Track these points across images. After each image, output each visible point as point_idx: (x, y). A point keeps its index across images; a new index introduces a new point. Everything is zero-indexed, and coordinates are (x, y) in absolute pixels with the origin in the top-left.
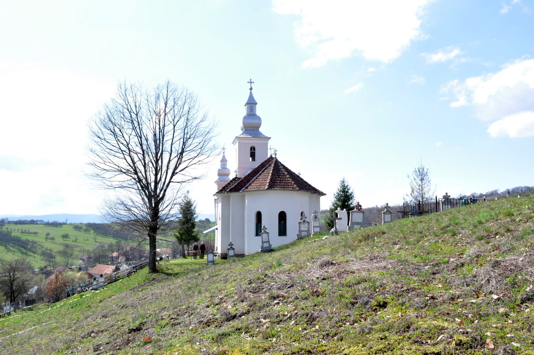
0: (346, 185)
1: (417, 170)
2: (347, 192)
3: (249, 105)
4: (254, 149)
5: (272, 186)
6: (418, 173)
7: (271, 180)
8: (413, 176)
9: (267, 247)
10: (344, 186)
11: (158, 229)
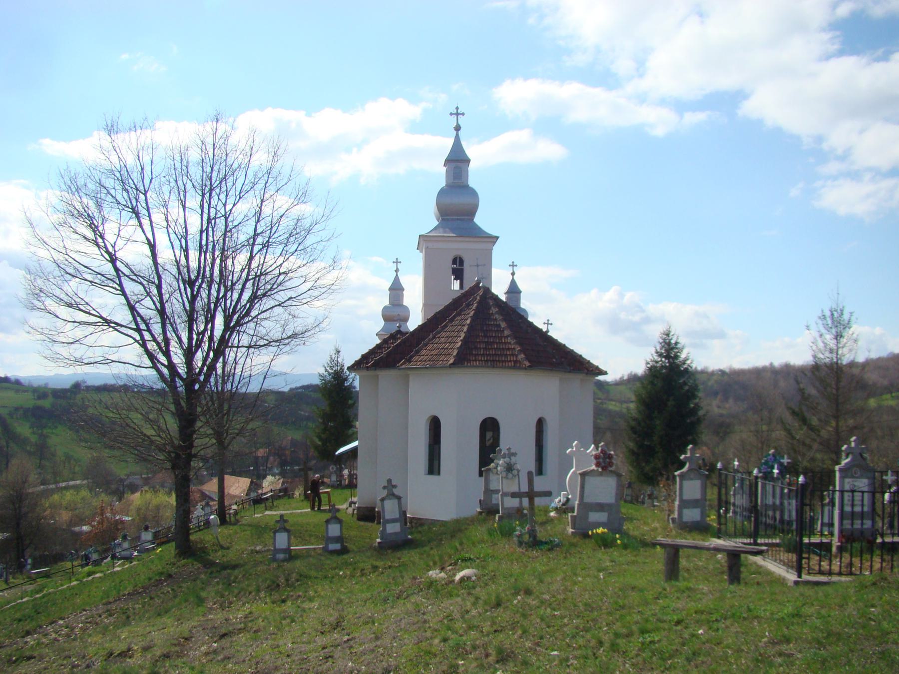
0: (673, 342)
1: (828, 314)
2: (676, 357)
3: (453, 165)
4: (461, 262)
5: (463, 359)
6: (829, 322)
7: (464, 341)
8: (817, 327)
9: (396, 534)
10: (669, 344)
11: (195, 456)
